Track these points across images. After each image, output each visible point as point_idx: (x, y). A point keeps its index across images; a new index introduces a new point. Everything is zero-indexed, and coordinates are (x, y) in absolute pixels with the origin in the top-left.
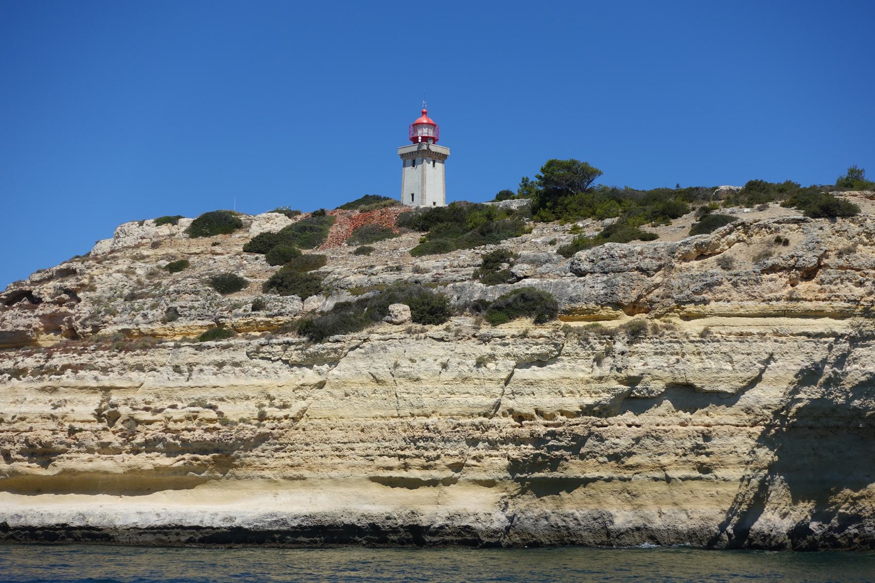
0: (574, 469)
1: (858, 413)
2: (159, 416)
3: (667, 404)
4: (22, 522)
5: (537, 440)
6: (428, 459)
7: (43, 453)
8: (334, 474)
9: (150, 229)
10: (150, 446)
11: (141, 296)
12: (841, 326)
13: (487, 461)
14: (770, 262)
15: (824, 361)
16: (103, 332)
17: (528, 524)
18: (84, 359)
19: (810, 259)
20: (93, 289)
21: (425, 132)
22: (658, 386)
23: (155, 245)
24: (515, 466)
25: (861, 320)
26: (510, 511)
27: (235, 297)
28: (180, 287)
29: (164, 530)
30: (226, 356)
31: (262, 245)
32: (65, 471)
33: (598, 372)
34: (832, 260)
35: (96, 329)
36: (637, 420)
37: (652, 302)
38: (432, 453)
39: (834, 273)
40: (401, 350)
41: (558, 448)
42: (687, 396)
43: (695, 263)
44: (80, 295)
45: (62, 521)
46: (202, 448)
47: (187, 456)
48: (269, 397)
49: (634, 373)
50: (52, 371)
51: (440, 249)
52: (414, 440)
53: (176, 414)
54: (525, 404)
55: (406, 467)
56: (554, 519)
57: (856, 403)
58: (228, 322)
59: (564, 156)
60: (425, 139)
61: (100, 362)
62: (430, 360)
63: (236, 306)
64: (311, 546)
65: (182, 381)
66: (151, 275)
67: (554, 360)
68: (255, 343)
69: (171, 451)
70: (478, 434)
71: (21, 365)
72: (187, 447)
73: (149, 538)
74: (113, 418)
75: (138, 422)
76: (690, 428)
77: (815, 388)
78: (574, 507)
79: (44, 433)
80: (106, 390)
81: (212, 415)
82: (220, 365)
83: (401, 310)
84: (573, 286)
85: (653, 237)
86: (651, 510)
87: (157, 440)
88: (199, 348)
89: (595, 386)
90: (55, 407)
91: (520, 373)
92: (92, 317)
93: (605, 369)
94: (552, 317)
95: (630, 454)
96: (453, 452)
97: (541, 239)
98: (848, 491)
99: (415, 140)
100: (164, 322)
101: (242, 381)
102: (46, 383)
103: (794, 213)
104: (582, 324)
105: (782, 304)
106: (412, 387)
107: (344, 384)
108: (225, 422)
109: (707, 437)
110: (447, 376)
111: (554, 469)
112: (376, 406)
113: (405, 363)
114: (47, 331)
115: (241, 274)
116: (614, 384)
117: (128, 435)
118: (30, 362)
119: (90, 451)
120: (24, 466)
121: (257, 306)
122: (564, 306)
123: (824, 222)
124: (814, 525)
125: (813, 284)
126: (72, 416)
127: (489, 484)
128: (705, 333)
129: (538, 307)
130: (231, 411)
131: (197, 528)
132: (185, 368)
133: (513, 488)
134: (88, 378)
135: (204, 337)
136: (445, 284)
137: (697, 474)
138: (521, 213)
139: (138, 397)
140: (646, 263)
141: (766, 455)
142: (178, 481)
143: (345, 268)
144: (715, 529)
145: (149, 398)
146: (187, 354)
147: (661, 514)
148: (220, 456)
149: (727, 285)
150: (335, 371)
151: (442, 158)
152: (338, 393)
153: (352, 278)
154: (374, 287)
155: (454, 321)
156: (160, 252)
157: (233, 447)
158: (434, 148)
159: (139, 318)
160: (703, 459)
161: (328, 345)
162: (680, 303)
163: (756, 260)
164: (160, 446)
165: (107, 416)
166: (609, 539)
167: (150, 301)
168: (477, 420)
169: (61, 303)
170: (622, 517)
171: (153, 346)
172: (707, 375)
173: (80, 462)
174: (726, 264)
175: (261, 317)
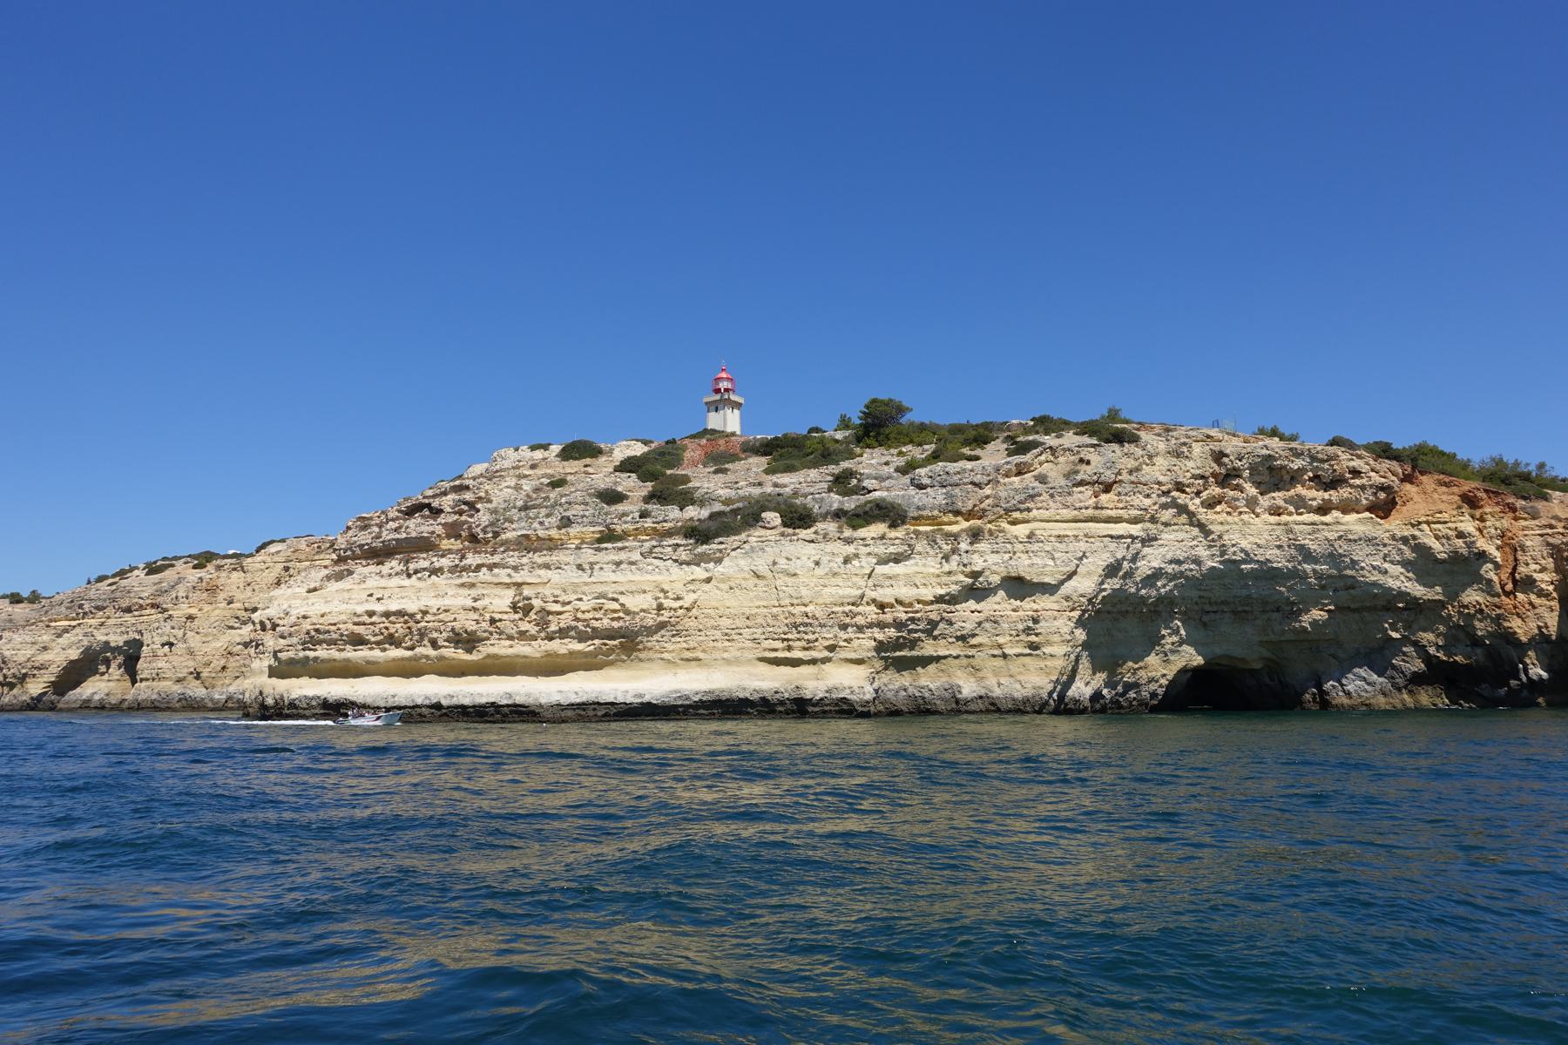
0: (928, 648)
1: (1143, 599)
2: (568, 608)
3: (1001, 593)
4: (455, 701)
5: (899, 625)
6: (809, 641)
7: (468, 641)
8: (726, 655)
9: (525, 453)
10: (563, 633)
11: (534, 507)
12: (1136, 530)
13: (855, 643)
14: (1079, 478)
15: (1124, 558)
16: (503, 537)
17: (889, 695)
18: (497, 559)
19: (1109, 476)
20: (490, 501)
21: (723, 385)
22: (995, 579)
23: (533, 467)
24: (881, 647)
25: (1149, 525)
26: (876, 685)
27: (620, 508)
28: (571, 498)
29: (582, 706)
30: (623, 556)
31: (628, 466)
32: (489, 656)
33: (946, 568)
34: (1125, 476)
35: (496, 535)
36: (978, 607)
37: (984, 510)
38: (811, 637)
39: (1128, 488)
40: (777, 550)
41: (916, 631)
42: (1018, 586)
43: (1016, 479)
44: (479, 506)
45: (492, 700)
46: (610, 634)
47: (596, 642)
48: (662, 590)
49: (977, 569)
50: (466, 569)
51: (790, 469)
52: (796, 626)
53: (583, 606)
54: (886, 595)
55: (789, 648)
56: (911, 690)
57: (1143, 592)
58: (618, 528)
59: (883, 396)
60: (727, 390)
61: (511, 562)
62: (804, 558)
63: (625, 514)
64: (711, 717)
65: (585, 577)
66: (537, 490)
67: (908, 557)
68: (647, 545)
69: (582, 637)
70: (848, 620)
71: (437, 565)
72: (596, 634)
73: (569, 713)
74: (527, 610)
75: (549, 613)
76: (1021, 613)
77: (1115, 580)
78: (928, 681)
79: (467, 623)
80: (519, 585)
81: (616, 606)
82: (618, 564)
83: (772, 517)
84: (917, 497)
85: (977, 458)
86: (991, 682)
87: (570, 628)
88: (599, 550)
89: (945, 579)
90: (475, 600)
91: (880, 569)
92: (492, 524)
93: (953, 564)
94: (904, 523)
95: (974, 636)
96: (829, 634)
97: (871, 462)
98: (1130, 664)
99: (718, 391)
100: (559, 528)
101: (637, 577)
102: (464, 580)
103: (1086, 440)
104: (928, 528)
105: (1090, 512)
106: (790, 580)
107: (729, 579)
108: (628, 612)
109: (1036, 621)
110: (819, 571)
111: (912, 649)
112: (758, 598)
113: (782, 562)
114: (449, 537)
115: (620, 489)
116: (962, 578)
117: (543, 624)
118: (445, 562)
119: (510, 638)
120: (449, 652)
121: (644, 515)
122: (913, 513)
123: (1115, 446)
124: (1105, 692)
125: (1111, 496)
126: (491, 608)
127: (859, 662)
128: (1031, 536)
129: (891, 514)
130: (632, 602)
131: (612, 704)
132: (587, 567)
133: (879, 665)
134: (502, 575)
135: (600, 541)
136: (805, 496)
137: (1028, 651)
138: (846, 441)
139: (547, 591)
140: (978, 479)
141: (1081, 635)
142: (589, 663)
143: (716, 487)
144: (1045, 696)
145: (557, 592)
146: (588, 555)
147: (999, 684)
148: (626, 642)
149: (1045, 496)
150: (720, 568)
151: (737, 405)
152: (725, 586)
153: (721, 492)
154: (742, 499)
155: (820, 526)
156: (539, 472)
157: (637, 634)
158: (733, 397)
159: (536, 525)
160: (1033, 638)
161: (714, 546)
162: (1007, 511)
163: (1067, 476)
164: (572, 633)
165: (522, 608)
166: (958, 707)
167: (543, 511)
168: (847, 608)
169: (461, 513)
170: (968, 688)
171: (556, 548)
172: (1035, 570)
173: (501, 648)
174: (1042, 479)
175: (648, 523)
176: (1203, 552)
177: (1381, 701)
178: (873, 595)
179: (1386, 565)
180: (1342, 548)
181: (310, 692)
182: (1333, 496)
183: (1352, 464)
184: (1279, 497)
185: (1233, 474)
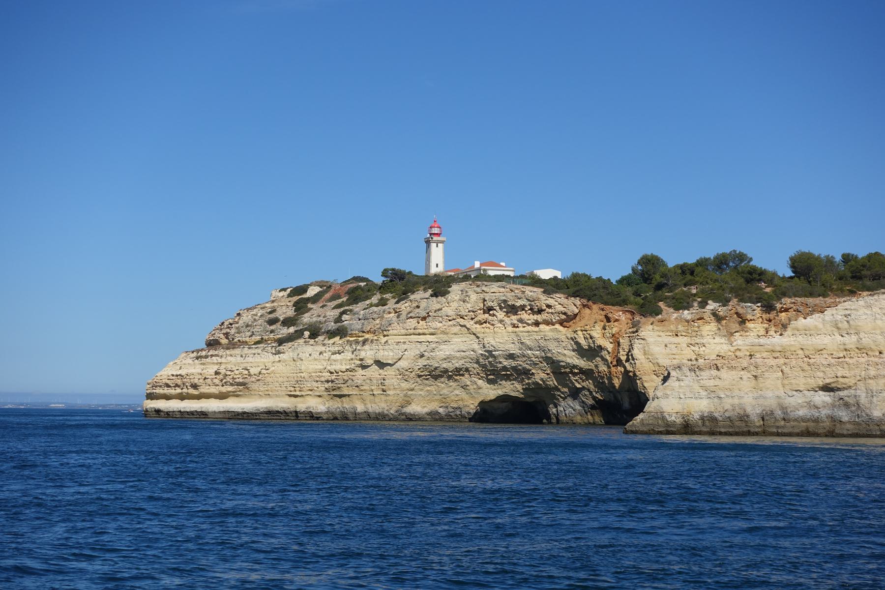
0: (345, 391)
18: (216, 353)
53: (237, 372)
54: (332, 368)
86: (369, 406)
91: (334, 357)
105: (412, 331)
110: (310, 358)
148: (243, 387)
151: (442, 242)
170: (360, 408)
173: (204, 389)
176: (476, 346)
177: (578, 419)
178: (329, 368)
179: (565, 352)
180: (542, 343)
181: (152, 406)
182: (539, 318)
183: (547, 302)
184: (514, 318)
185: (490, 309)
